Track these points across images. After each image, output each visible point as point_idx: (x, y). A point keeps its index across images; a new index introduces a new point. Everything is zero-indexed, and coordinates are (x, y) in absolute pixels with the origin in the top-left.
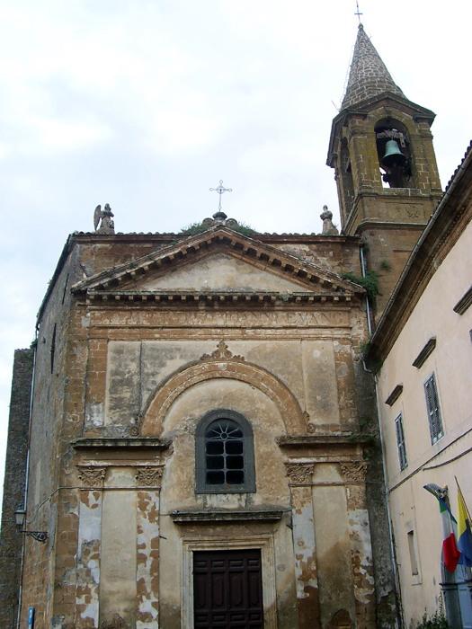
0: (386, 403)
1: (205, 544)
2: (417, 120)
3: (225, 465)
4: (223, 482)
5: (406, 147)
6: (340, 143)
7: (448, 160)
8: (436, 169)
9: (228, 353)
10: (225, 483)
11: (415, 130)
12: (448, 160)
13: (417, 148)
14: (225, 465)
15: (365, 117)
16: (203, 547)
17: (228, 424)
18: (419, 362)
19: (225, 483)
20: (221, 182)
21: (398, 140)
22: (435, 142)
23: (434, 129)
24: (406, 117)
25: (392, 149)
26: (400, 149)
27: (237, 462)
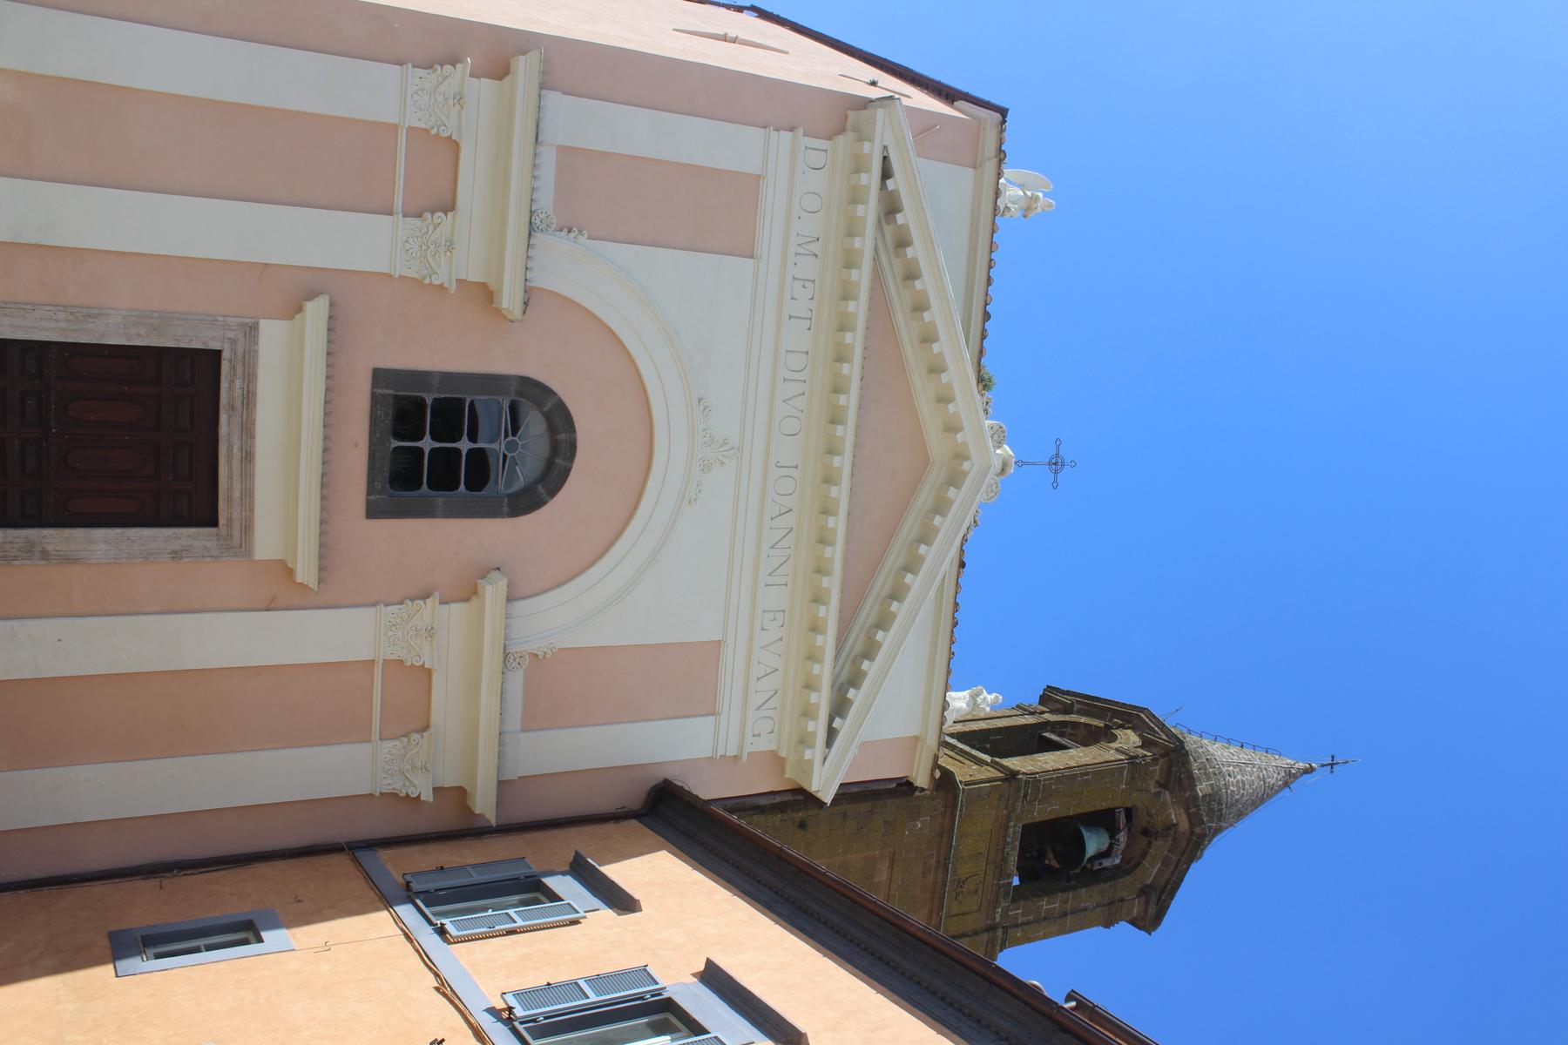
0: (709, 963)
1: (238, 383)
2: (1144, 892)
3: (437, 445)
4: (398, 435)
5: (1093, 875)
6: (1101, 724)
7: (1057, 963)
8: (1045, 937)
9: (706, 468)
10: (429, 402)
11: (1125, 887)
12: (1057, 963)
13: (1088, 896)
14: (437, 445)
15: (1164, 785)
16: (229, 462)
17: (527, 469)
18: (714, 978)
19: (429, 402)
20: (1074, 464)
21: (1106, 854)
22: (1098, 931)
23: (1123, 930)
24: (1151, 871)
25: (1094, 843)
26: (1091, 859)
27: (444, 473)
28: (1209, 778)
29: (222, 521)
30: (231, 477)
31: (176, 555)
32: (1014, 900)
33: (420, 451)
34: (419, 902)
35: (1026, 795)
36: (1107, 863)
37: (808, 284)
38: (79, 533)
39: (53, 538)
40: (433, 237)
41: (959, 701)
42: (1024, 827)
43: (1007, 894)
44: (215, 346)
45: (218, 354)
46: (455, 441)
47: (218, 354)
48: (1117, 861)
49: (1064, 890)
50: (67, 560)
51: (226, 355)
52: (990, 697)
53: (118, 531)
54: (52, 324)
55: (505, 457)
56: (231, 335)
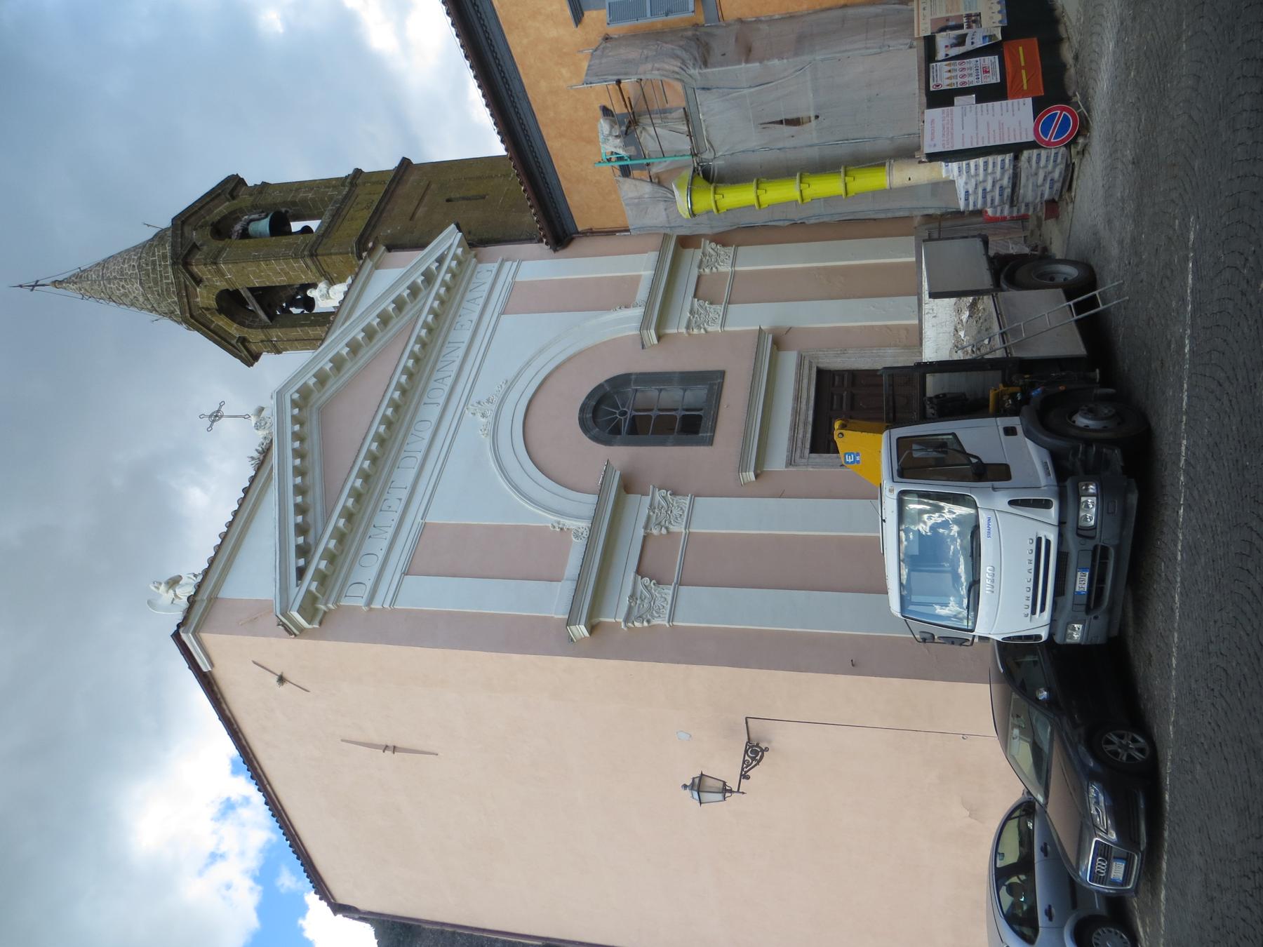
29: (814, 370)
51: (807, 451)
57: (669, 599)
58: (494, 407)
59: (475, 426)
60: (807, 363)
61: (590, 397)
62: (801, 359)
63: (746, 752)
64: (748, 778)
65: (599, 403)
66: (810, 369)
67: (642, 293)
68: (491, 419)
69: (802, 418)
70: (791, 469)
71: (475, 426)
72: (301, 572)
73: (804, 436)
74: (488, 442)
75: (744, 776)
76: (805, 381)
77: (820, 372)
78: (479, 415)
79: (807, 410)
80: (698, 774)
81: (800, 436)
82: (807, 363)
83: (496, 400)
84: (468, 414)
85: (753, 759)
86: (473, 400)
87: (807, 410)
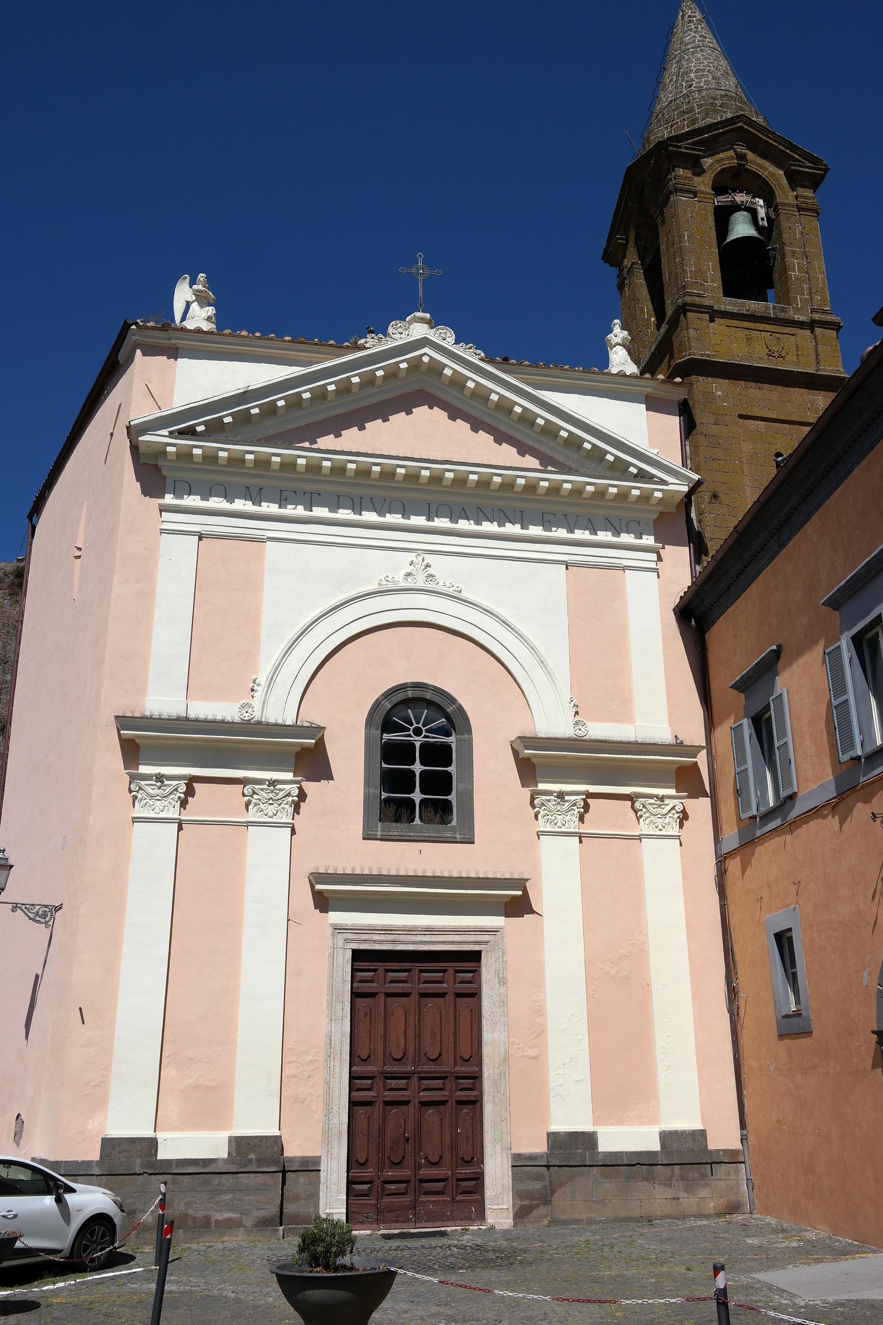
25: (741, 228)
27: (439, 783)
28: (691, 110)
29: (476, 948)
30: (444, 943)
31: (503, 982)
32: (789, 303)
33: (423, 802)
34: (339, 1295)
35: (699, 295)
36: (762, 213)
37: (284, 497)
38: (486, 1050)
39: (489, 1071)
40: (740, 1238)
41: (620, 361)
42: (726, 294)
43: (783, 310)
44: (349, 955)
45: (355, 952)
46: (425, 799)
47: (355, 952)
48: (761, 202)
49: (783, 256)
50: (506, 1060)
51: (355, 946)
52: (617, 329)
53: (484, 1022)
54: (337, 1070)
55: (425, 737)
56: (340, 944)
57: (162, 815)
58: (420, 584)
59: (395, 567)
60: (486, 938)
61: (437, 691)
62: (494, 931)
63: (46, 906)
64: (14, 910)
65: (430, 704)
66: (476, 943)
67: (597, 730)
68: (403, 584)
69: (402, 938)
70: (330, 930)
71: (395, 567)
72: (190, 433)
73: (375, 941)
74: (374, 587)
75: (15, 907)
76: (457, 938)
77: (475, 956)
78: (409, 569)
79: (413, 943)
80: (11, 862)
81: (376, 937)
82: (486, 938)
83: (431, 586)
84: (412, 556)
85: (37, 914)
86: (429, 558)
87: (413, 943)
